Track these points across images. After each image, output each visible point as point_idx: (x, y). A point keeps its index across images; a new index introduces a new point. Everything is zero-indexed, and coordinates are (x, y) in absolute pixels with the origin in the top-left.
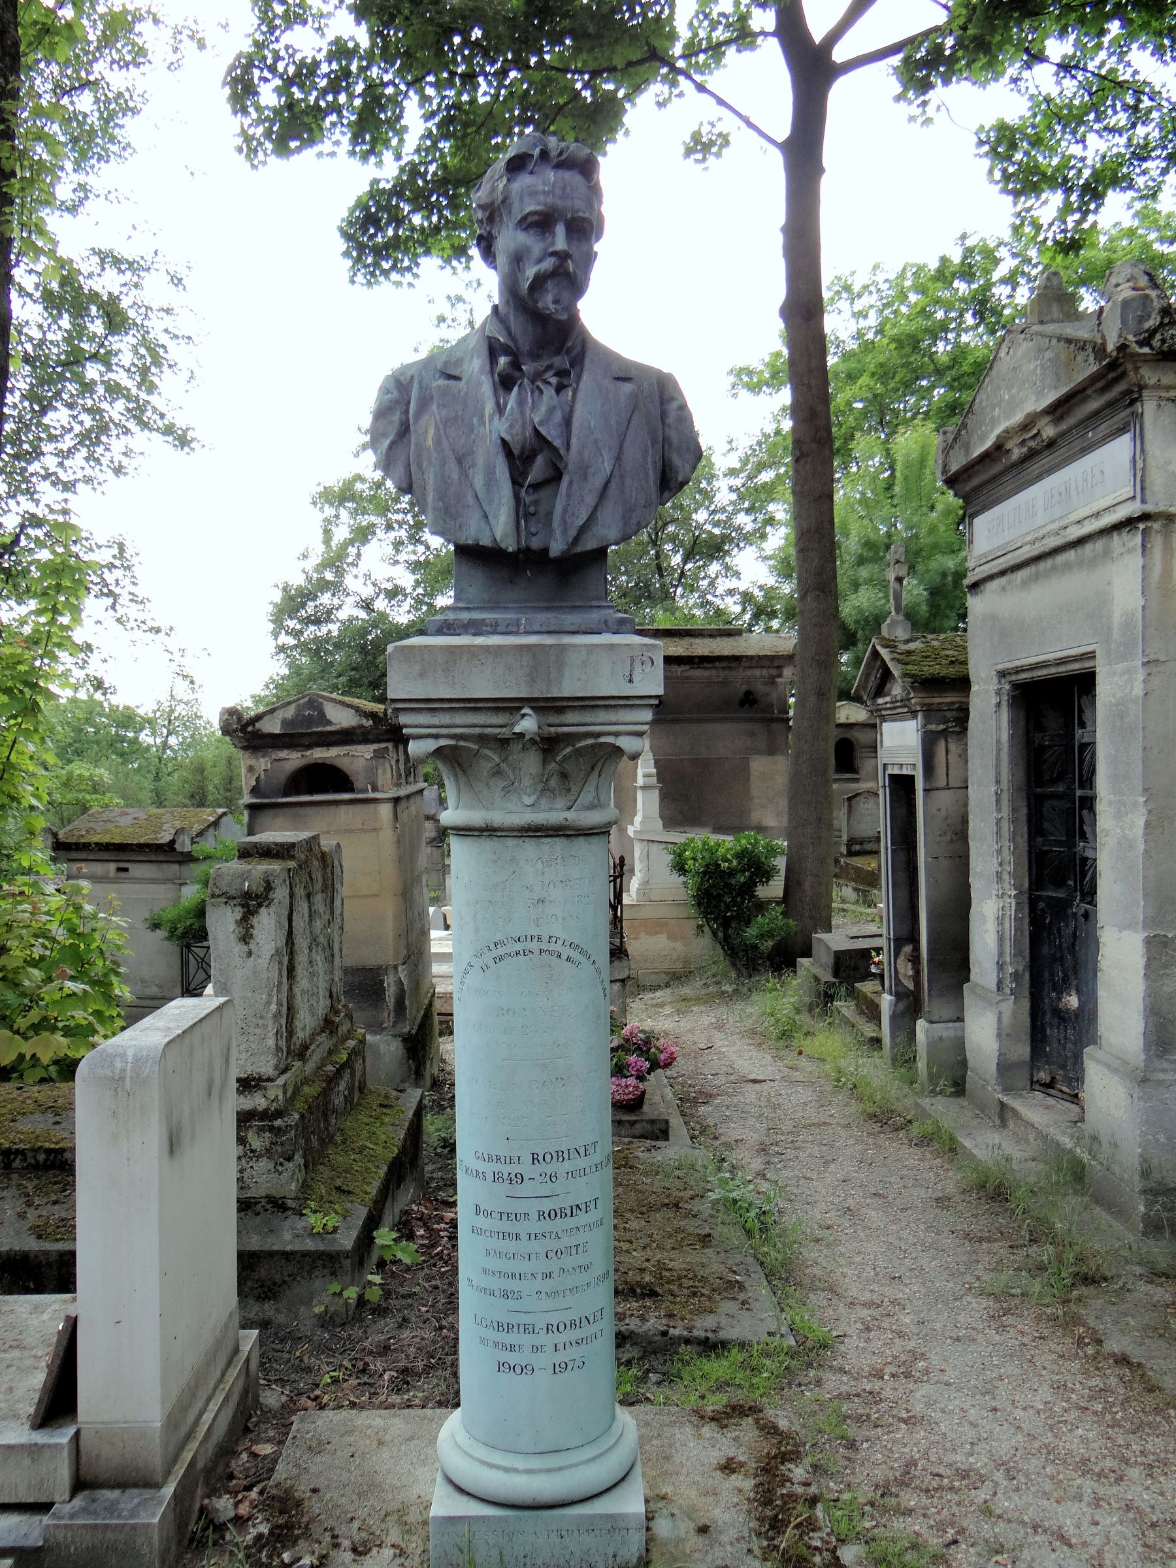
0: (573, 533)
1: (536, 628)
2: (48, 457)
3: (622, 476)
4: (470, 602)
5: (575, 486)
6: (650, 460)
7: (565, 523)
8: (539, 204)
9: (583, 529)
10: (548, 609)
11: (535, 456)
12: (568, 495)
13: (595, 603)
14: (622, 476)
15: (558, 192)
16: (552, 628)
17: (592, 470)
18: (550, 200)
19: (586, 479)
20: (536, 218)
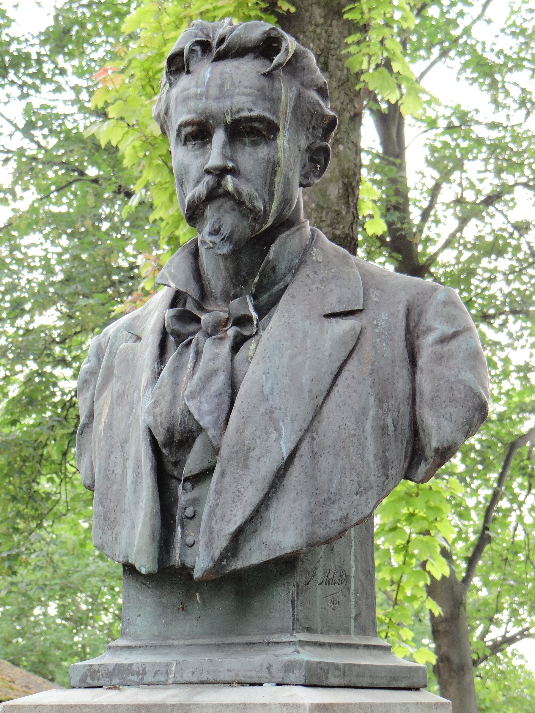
0: (221, 543)
1: (187, 677)
2: (441, 259)
3: (314, 455)
4: (136, 637)
5: (228, 479)
6: (369, 425)
7: (211, 532)
8: (189, 112)
9: (238, 538)
10: (218, 647)
11: (194, 439)
12: (218, 492)
13: (275, 638)
14: (314, 455)
15: (214, 91)
16: (205, 677)
17: (256, 453)
18: (201, 105)
19: (246, 467)
20: (189, 129)
